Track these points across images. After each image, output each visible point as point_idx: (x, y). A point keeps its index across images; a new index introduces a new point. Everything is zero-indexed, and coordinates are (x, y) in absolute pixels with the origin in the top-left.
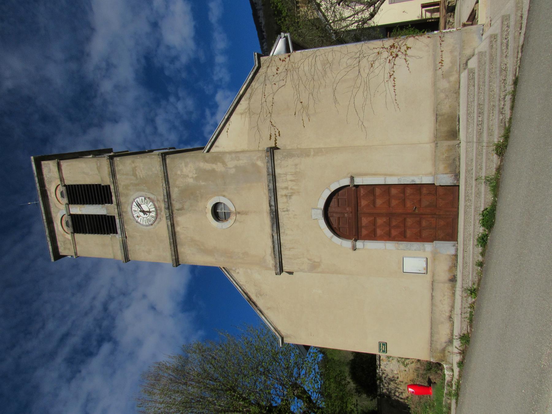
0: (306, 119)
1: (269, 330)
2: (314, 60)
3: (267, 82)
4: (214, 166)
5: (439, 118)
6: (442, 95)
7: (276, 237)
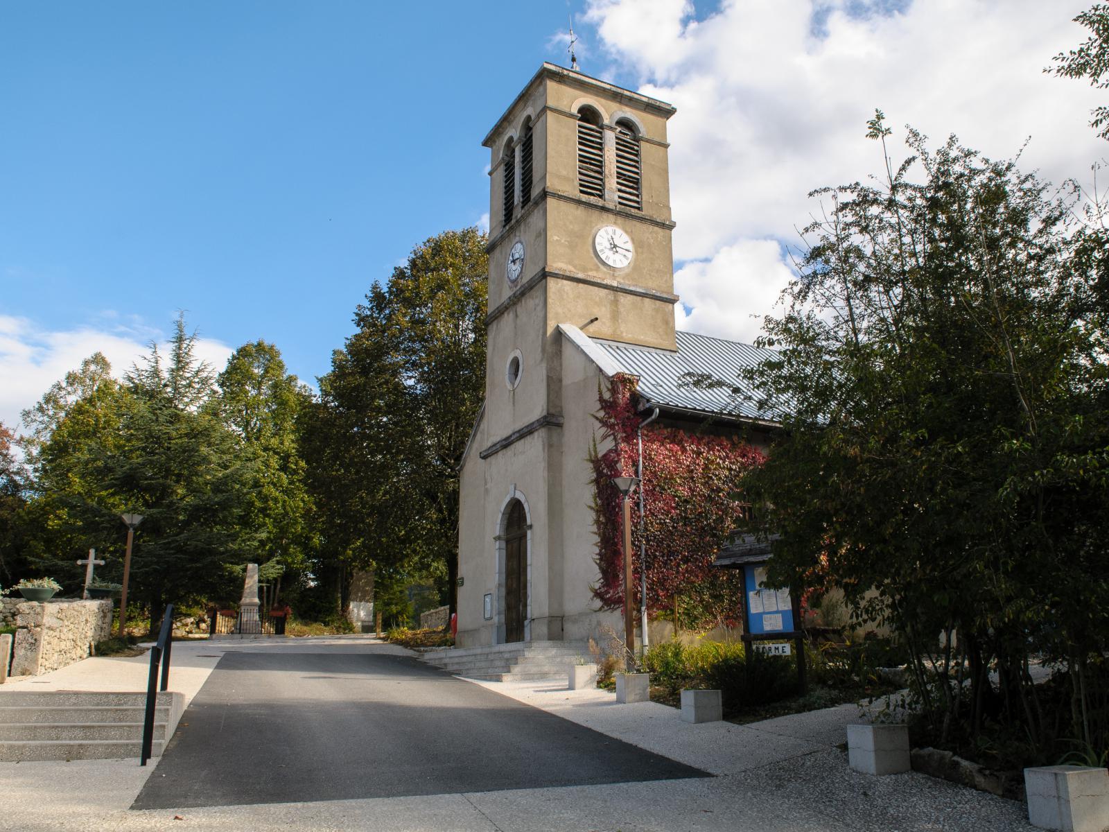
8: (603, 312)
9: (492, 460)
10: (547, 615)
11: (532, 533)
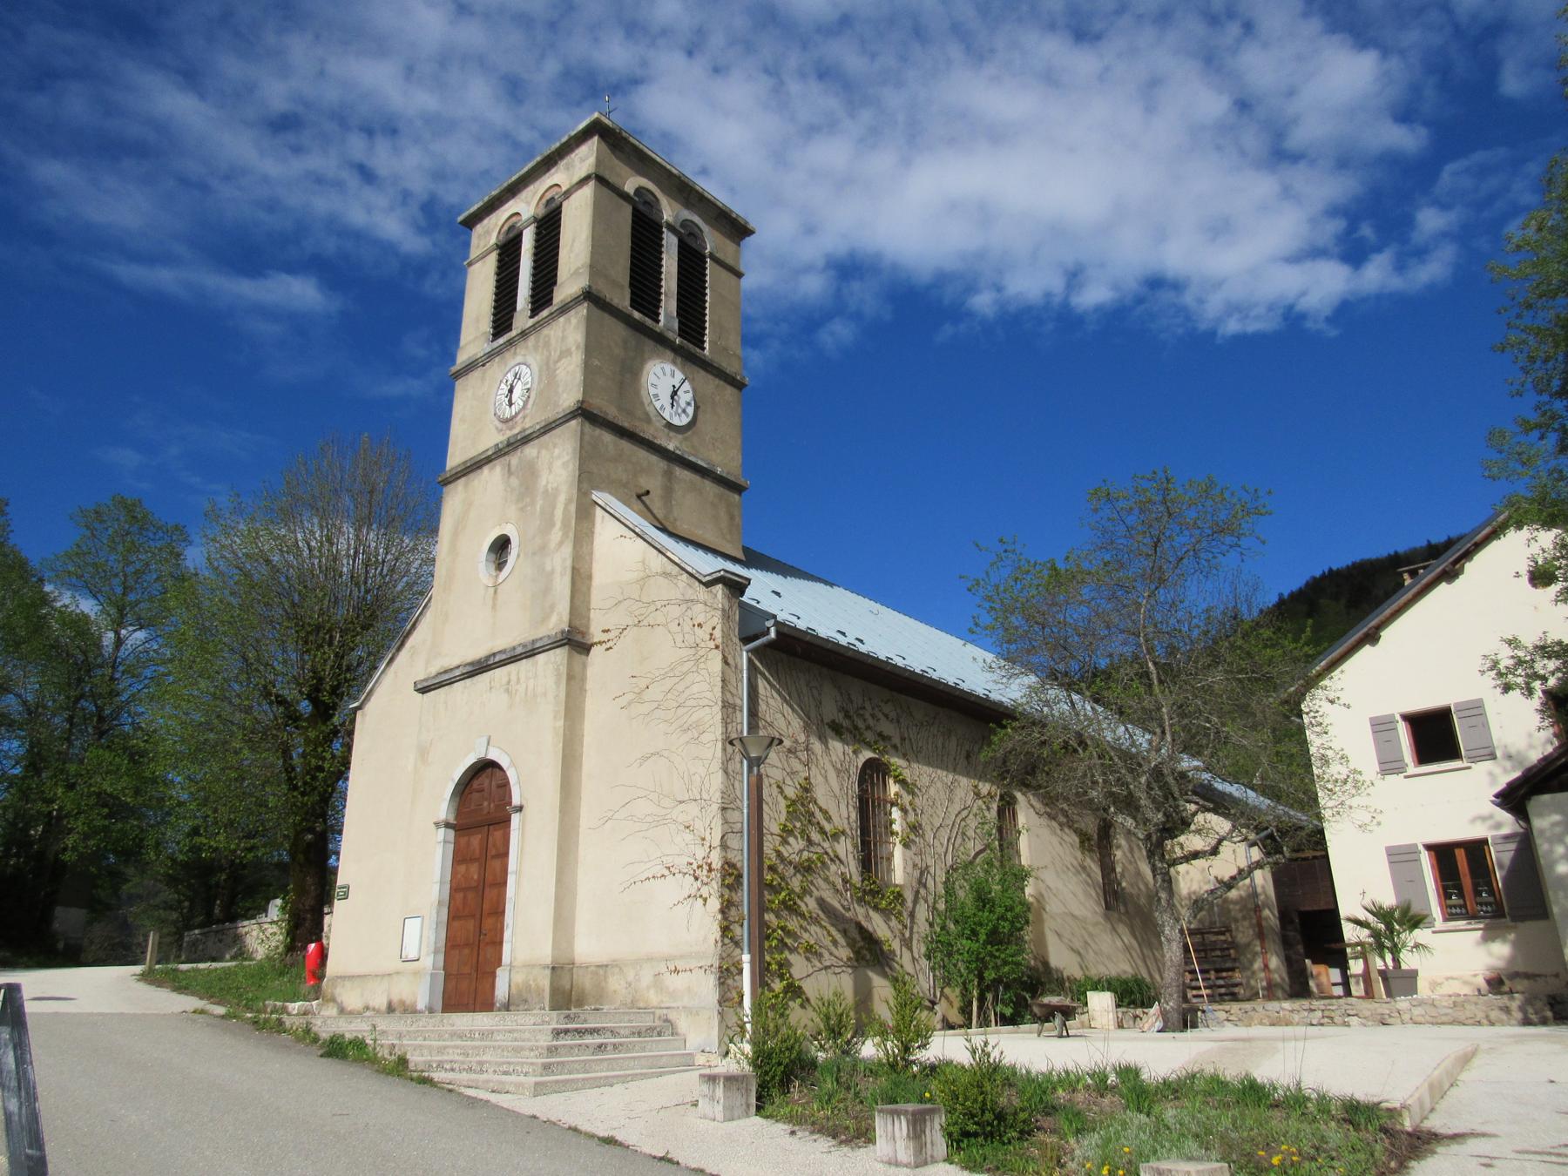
0: (623, 701)
1: (367, 682)
2: (706, 702)
3: (684, 607)
4: (558, 524)
5: (601, 972)
6: (631, 976)
7: (457, 673)
8: (653, 483)
9: (738, 208)
10: (548, 961)
11: (523, 823)
